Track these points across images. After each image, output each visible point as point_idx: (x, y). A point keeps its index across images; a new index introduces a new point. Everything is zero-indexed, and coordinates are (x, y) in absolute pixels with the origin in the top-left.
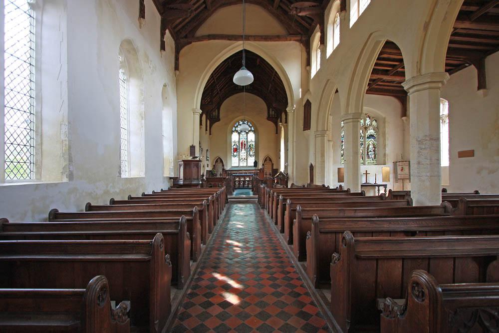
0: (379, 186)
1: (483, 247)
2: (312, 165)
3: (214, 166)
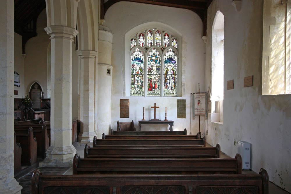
3: (30, 93)
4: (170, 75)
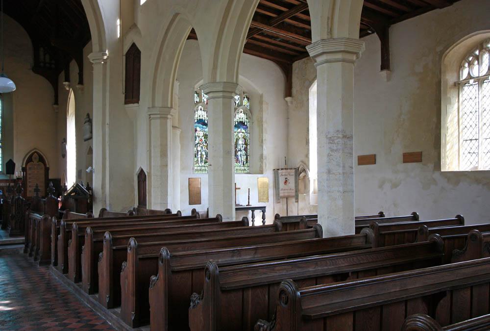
0: (253, 209)
1: (430, 282)
2: (142, 171)
4: (242, 145)
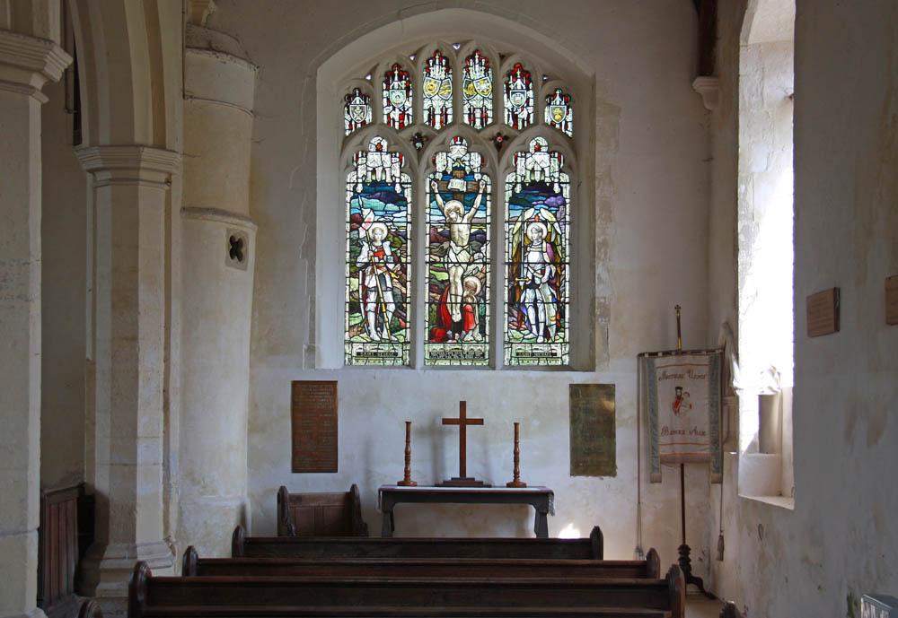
4: (539, 267)
